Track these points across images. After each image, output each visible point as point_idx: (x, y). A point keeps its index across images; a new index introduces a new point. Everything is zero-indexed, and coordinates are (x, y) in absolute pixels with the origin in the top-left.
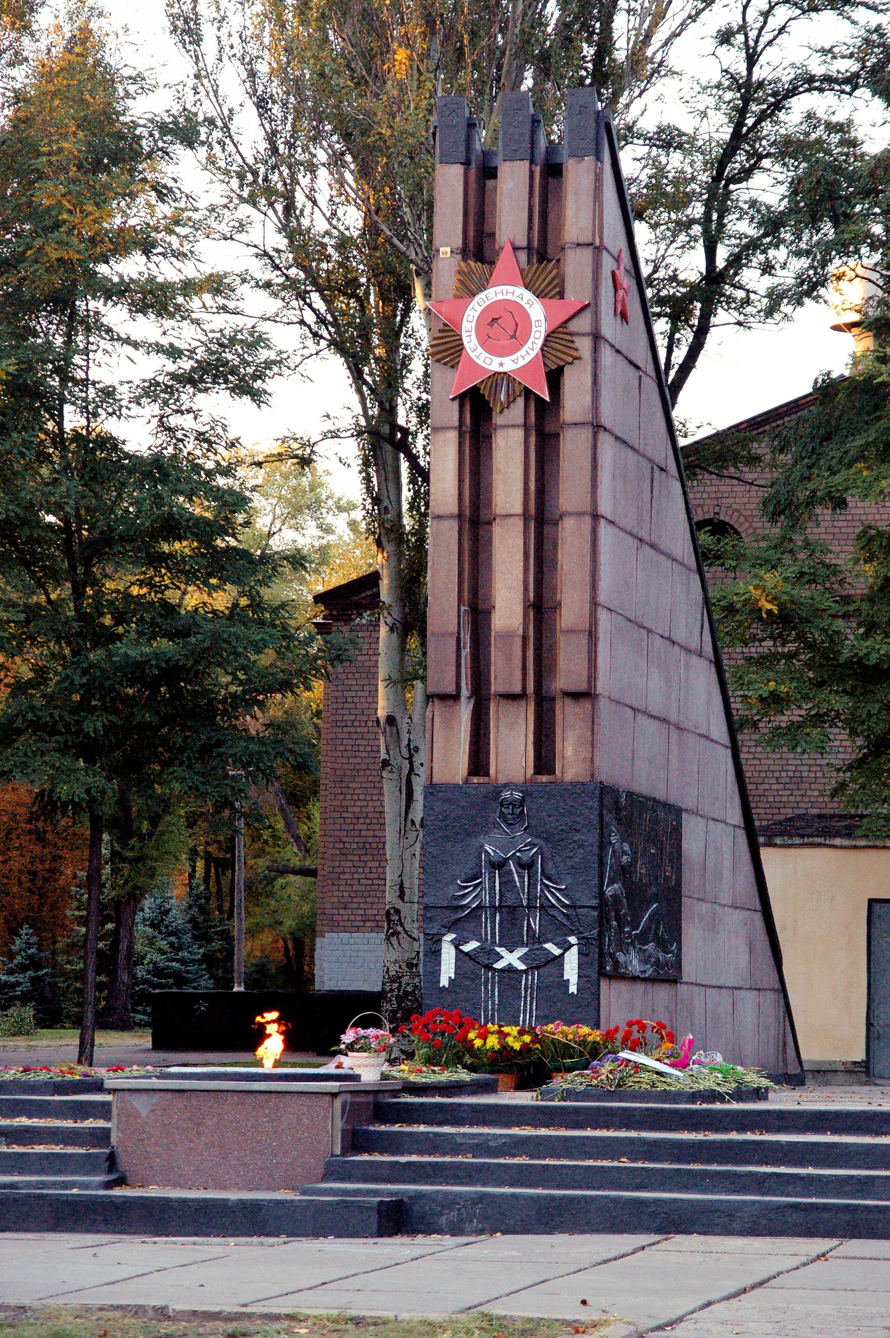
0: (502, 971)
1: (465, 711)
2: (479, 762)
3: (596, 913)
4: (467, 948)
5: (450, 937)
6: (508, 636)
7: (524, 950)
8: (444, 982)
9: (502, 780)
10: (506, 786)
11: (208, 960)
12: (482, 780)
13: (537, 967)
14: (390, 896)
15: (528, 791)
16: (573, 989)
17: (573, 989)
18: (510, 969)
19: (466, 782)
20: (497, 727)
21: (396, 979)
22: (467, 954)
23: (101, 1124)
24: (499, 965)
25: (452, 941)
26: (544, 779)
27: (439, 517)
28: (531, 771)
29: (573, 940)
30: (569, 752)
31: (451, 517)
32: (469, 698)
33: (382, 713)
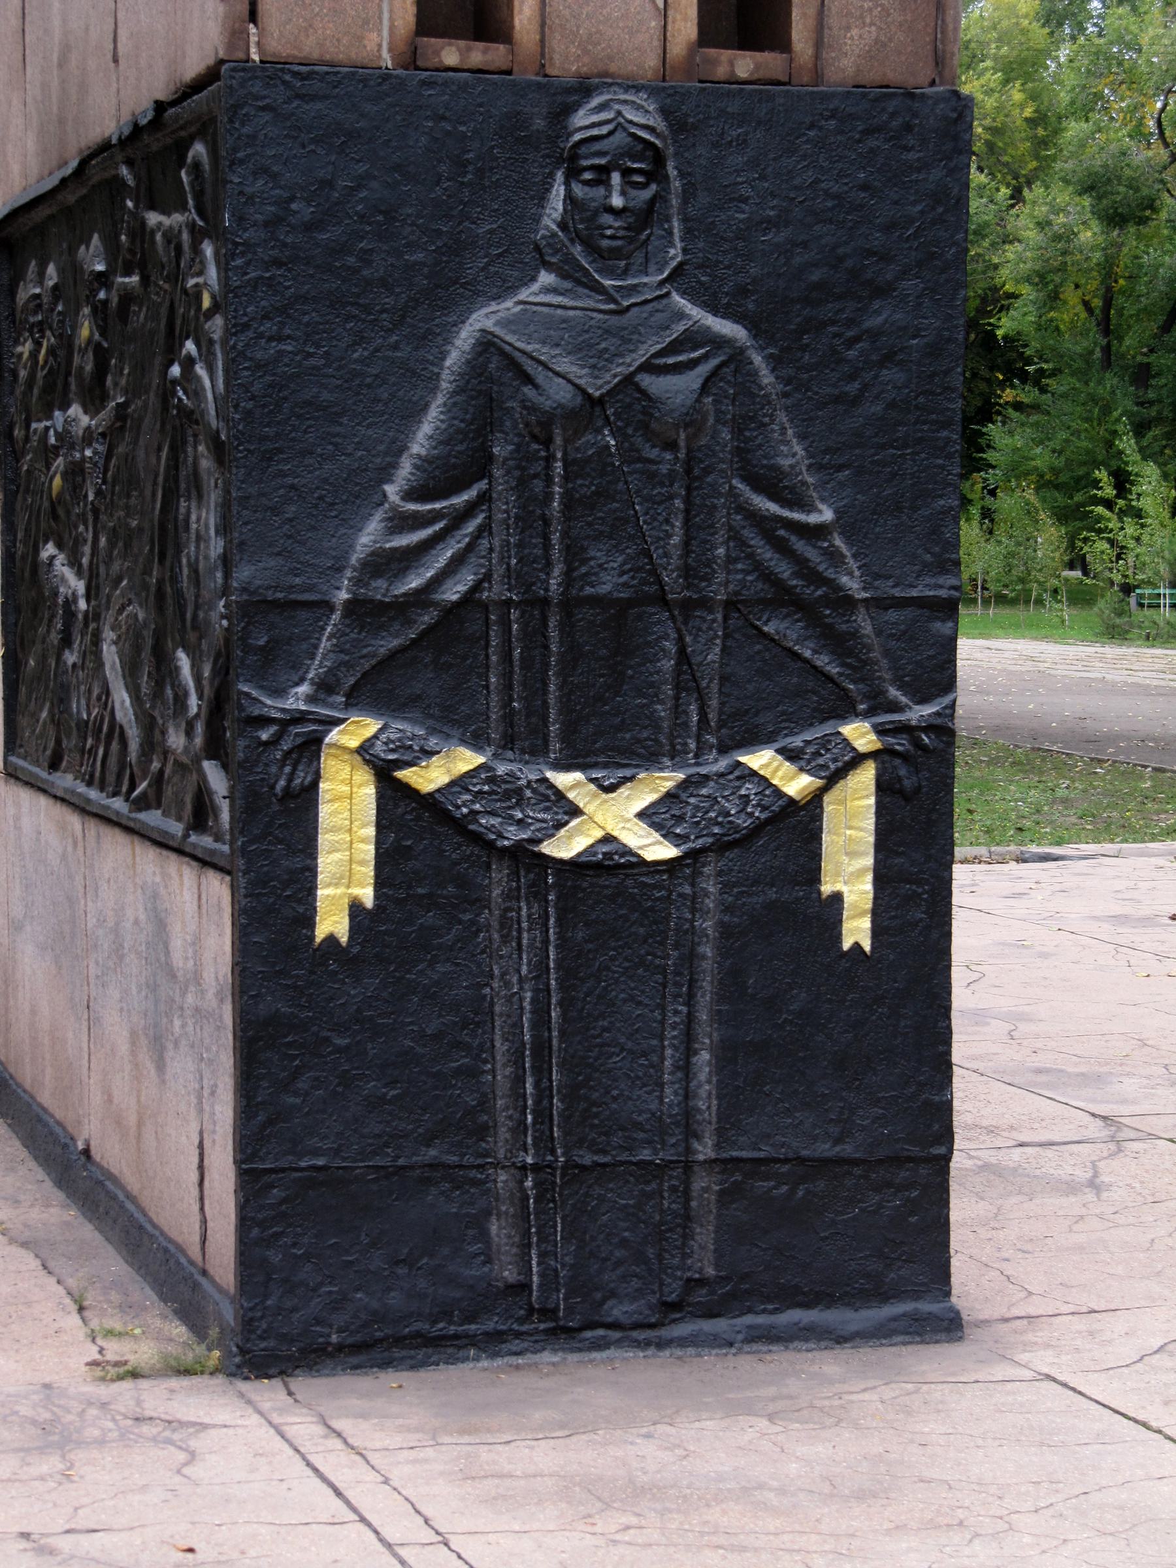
0: (575, 866)
4: (429, 777)
5: (357, 730)
7: (666, 780)
8: (333, 923)
9: (567, 61)
10: (583, 89)
12: (479, 54)
15: (682, 97)
16: (857, 930)
17: (857, 930)
18: (609, 863)
19: (411, 58)
22: (430, 803)
24: (567, 846)
25: (364, 750)
26: (745, 64)
29: (860, 734)
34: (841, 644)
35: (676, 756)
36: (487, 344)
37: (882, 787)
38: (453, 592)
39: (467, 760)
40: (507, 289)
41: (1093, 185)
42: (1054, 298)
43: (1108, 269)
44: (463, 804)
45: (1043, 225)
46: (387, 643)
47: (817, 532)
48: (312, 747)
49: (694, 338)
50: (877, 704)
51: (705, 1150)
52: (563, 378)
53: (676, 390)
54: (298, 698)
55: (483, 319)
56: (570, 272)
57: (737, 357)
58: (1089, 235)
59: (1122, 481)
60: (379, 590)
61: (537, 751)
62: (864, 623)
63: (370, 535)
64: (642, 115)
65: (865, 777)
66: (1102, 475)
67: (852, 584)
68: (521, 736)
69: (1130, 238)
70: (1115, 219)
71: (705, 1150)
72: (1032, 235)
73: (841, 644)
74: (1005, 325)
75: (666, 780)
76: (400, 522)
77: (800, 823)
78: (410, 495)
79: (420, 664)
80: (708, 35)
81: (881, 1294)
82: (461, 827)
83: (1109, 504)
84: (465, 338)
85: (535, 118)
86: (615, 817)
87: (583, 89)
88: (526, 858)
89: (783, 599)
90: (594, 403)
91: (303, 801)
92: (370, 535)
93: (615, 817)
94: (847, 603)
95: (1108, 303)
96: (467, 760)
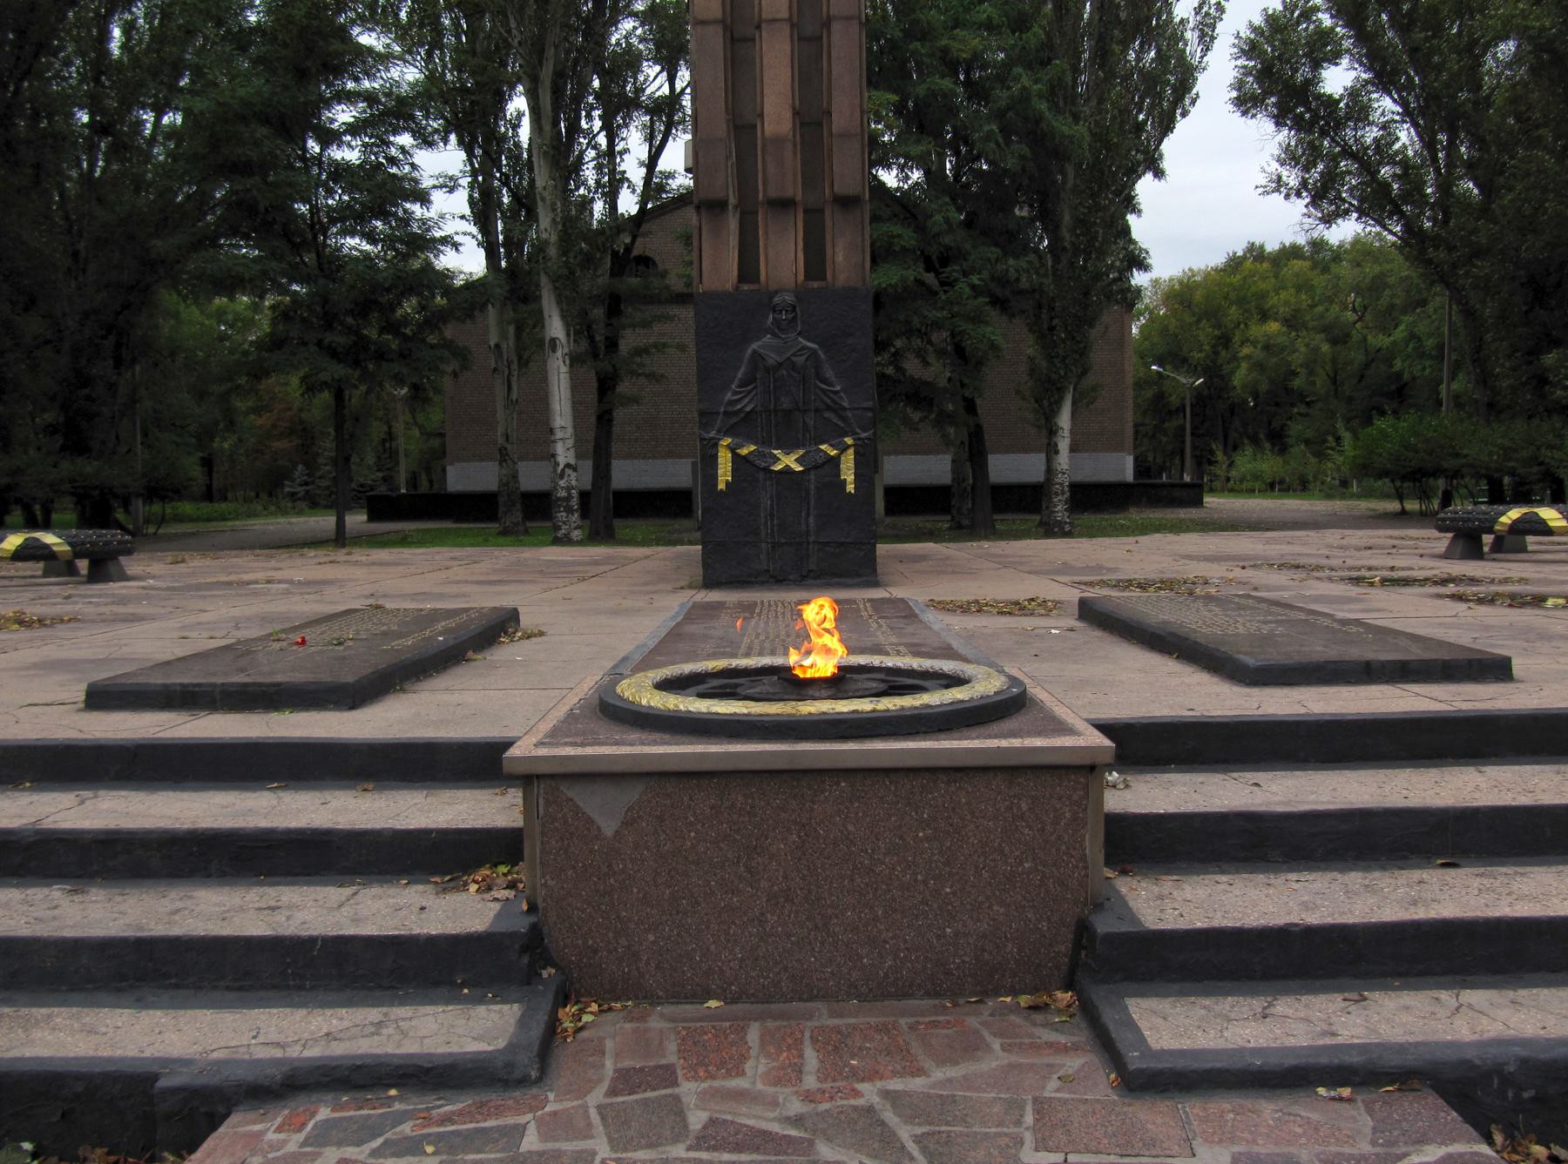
0: (780, 472)
1: (733, 223)
2: (748, 270)
3: (870, 414)
4: (744, 451)
5: (726, 441)
6: (778, 141)
7: (801, 452)
8: (721, 486)
9: (773, 287)
10: (776, 292)
11: (385, 479)
12: (752, 287)
13: (816, 468)
14: (501, 440)
15: (801, 294)
16: (850, 488)
17: (850, 488)
18: (787, 471)
19: (737, 288)
20: (766, 233)
21: (507, 484)
22: (744, 458)
23: (593, 1113)
24: (778, 467)
25: (728, 446)
26: (816, 285)
27: (703, 23)
28: (801, 277)
29: (849, 441)
30: (840, 258)
31: (715, 22)
32: (736, 207)
33: (492, 344)
34: (844, 419)
35: (804, 446)
36: (755, 352)
37: (856, 453)
38: (748, 409)
39: (753, 448)
40: (759, 339)
41: (1325, 329)
42: (1311, 373)
43: (1334, 360)
44: (751, 458)
45: (1307, 345)
46: (734, 420)
47: (836, 392)
48: (716, 445)
49: (804, 348)
50: (853, 434)
51: (811, 539)
52: (773, 358)
53: (800, 360)
54: (713, 434)
55: (754, 346)
56: (774, 335)
57: (814, 352)
58: (1325, 348)
59: (1338, 439)
60: (730, 409)
61: (770, 446)
62: (849, 414)
63: (729, 396)
64: (789, 298)
65: (851, 451)
66: (1330, 438)
67: (845, 404)
68: (766, 442)
69: (1338, 348)
70: (1334, 342)
71: (811, 539)
72: (1303, 349)
73: (844, 419)
74: (1297, 383)
75: (801, 452)
76: (736, 393)
77: (835, 462)
78: (740, 386)
79: (741, 426)
80: (807, 277)
81: (859, 575)
82: (752, 464)
83: (1332, 449)
84: (749, 351)
85: (766, 301)
86: (789, 461)
87: (776, 292)
88: (767, 470)
89: (829, 408)
90: (780, 364)
91: (715, 457)
92: (729, 396)
93: (789, 461)
94: (844, 409)
95: (1336, 373)
96: (753, 448)
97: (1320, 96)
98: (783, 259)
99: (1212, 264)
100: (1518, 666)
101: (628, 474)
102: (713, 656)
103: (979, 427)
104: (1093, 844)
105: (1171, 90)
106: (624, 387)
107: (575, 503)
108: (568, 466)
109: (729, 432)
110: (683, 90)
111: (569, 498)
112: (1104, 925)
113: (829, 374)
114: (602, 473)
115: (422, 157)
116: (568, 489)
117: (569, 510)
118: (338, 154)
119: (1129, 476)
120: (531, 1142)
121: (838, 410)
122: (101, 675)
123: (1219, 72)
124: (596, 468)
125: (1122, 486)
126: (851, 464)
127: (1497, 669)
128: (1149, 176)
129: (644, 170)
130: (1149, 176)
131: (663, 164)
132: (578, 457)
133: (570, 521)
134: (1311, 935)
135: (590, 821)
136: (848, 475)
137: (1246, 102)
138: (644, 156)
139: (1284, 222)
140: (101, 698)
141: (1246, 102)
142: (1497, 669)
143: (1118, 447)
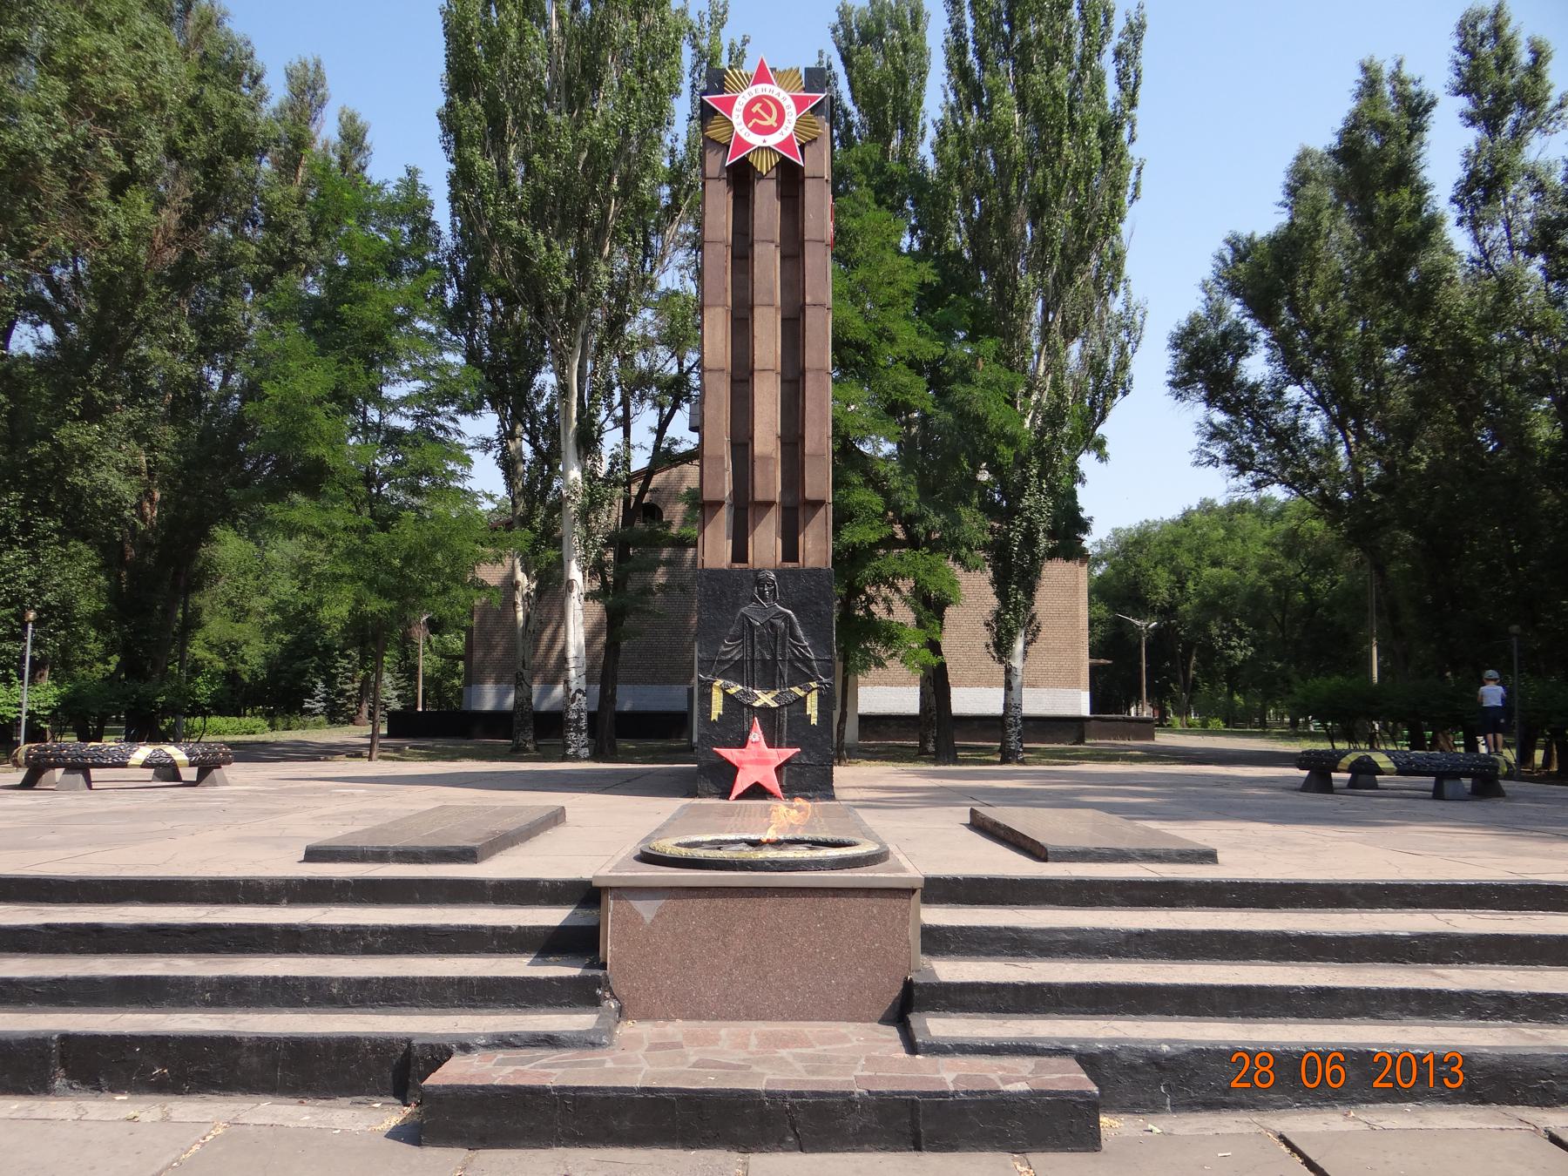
2: (740, 553)
4: (732, 691)
5: (719, 682)
8: (714, 717)
9: (757, 567)
12: (742, 566)
16: (814, 721)
17: (814, 721)
24: (757, 704)
28: (779, 559)
30: (809, 546)
54: (709, 677)
77: (802, 701)
79: (736, 671)
80: (785, 559)
85: (757, 579)
97: (1242, 384)
98: (766, 544)
99: (1166, 518)
100: (1219, 856)
101: (628, 700)
102: (709, 832)
103: (943, 666)
104: (916, 943)
105: (1107, 383)
106: (629, 622)
107: (583, 724)
108: (579, 691)
109: (723, 675)
110: (690, 370)
111: (580, 718)
112: (918, 979)
113: (800, 632)
114: (607, 698)
115: (465, 422)
116: (579, 711)
117: (579, 730)
118: (395, 421)
119: (1085, 711)
120: (609, 1065)
121: (806, 661)
122: (311, 843)
123: (1152, 363)
124: (603, 692)
125: (1080, 720)
126: (815, 703)
127: (1209, 857)
128: (1093, 455)
129: (654, 437)
130: (1093, 455)
131: (670, 432)
132: (588, 681)
133: (578, 741)
134: (1030, 987)
135: (638, 914)
136: (812, 709)
137: (1180, 385)
138: (655, 424)
139: (1220, 486)
140: (313, 855)
141: (1180, 385)
142: (1209, 857)
143: (1075, 684)
